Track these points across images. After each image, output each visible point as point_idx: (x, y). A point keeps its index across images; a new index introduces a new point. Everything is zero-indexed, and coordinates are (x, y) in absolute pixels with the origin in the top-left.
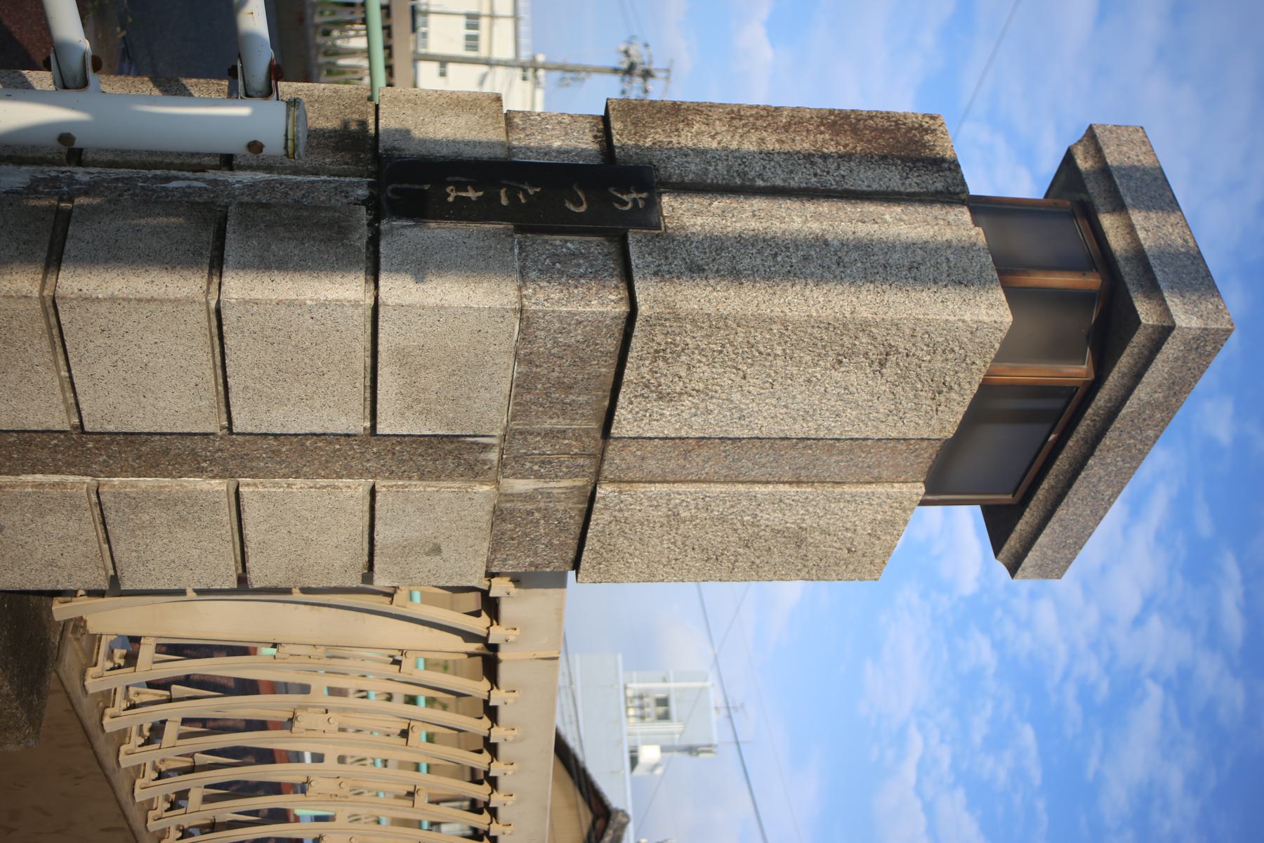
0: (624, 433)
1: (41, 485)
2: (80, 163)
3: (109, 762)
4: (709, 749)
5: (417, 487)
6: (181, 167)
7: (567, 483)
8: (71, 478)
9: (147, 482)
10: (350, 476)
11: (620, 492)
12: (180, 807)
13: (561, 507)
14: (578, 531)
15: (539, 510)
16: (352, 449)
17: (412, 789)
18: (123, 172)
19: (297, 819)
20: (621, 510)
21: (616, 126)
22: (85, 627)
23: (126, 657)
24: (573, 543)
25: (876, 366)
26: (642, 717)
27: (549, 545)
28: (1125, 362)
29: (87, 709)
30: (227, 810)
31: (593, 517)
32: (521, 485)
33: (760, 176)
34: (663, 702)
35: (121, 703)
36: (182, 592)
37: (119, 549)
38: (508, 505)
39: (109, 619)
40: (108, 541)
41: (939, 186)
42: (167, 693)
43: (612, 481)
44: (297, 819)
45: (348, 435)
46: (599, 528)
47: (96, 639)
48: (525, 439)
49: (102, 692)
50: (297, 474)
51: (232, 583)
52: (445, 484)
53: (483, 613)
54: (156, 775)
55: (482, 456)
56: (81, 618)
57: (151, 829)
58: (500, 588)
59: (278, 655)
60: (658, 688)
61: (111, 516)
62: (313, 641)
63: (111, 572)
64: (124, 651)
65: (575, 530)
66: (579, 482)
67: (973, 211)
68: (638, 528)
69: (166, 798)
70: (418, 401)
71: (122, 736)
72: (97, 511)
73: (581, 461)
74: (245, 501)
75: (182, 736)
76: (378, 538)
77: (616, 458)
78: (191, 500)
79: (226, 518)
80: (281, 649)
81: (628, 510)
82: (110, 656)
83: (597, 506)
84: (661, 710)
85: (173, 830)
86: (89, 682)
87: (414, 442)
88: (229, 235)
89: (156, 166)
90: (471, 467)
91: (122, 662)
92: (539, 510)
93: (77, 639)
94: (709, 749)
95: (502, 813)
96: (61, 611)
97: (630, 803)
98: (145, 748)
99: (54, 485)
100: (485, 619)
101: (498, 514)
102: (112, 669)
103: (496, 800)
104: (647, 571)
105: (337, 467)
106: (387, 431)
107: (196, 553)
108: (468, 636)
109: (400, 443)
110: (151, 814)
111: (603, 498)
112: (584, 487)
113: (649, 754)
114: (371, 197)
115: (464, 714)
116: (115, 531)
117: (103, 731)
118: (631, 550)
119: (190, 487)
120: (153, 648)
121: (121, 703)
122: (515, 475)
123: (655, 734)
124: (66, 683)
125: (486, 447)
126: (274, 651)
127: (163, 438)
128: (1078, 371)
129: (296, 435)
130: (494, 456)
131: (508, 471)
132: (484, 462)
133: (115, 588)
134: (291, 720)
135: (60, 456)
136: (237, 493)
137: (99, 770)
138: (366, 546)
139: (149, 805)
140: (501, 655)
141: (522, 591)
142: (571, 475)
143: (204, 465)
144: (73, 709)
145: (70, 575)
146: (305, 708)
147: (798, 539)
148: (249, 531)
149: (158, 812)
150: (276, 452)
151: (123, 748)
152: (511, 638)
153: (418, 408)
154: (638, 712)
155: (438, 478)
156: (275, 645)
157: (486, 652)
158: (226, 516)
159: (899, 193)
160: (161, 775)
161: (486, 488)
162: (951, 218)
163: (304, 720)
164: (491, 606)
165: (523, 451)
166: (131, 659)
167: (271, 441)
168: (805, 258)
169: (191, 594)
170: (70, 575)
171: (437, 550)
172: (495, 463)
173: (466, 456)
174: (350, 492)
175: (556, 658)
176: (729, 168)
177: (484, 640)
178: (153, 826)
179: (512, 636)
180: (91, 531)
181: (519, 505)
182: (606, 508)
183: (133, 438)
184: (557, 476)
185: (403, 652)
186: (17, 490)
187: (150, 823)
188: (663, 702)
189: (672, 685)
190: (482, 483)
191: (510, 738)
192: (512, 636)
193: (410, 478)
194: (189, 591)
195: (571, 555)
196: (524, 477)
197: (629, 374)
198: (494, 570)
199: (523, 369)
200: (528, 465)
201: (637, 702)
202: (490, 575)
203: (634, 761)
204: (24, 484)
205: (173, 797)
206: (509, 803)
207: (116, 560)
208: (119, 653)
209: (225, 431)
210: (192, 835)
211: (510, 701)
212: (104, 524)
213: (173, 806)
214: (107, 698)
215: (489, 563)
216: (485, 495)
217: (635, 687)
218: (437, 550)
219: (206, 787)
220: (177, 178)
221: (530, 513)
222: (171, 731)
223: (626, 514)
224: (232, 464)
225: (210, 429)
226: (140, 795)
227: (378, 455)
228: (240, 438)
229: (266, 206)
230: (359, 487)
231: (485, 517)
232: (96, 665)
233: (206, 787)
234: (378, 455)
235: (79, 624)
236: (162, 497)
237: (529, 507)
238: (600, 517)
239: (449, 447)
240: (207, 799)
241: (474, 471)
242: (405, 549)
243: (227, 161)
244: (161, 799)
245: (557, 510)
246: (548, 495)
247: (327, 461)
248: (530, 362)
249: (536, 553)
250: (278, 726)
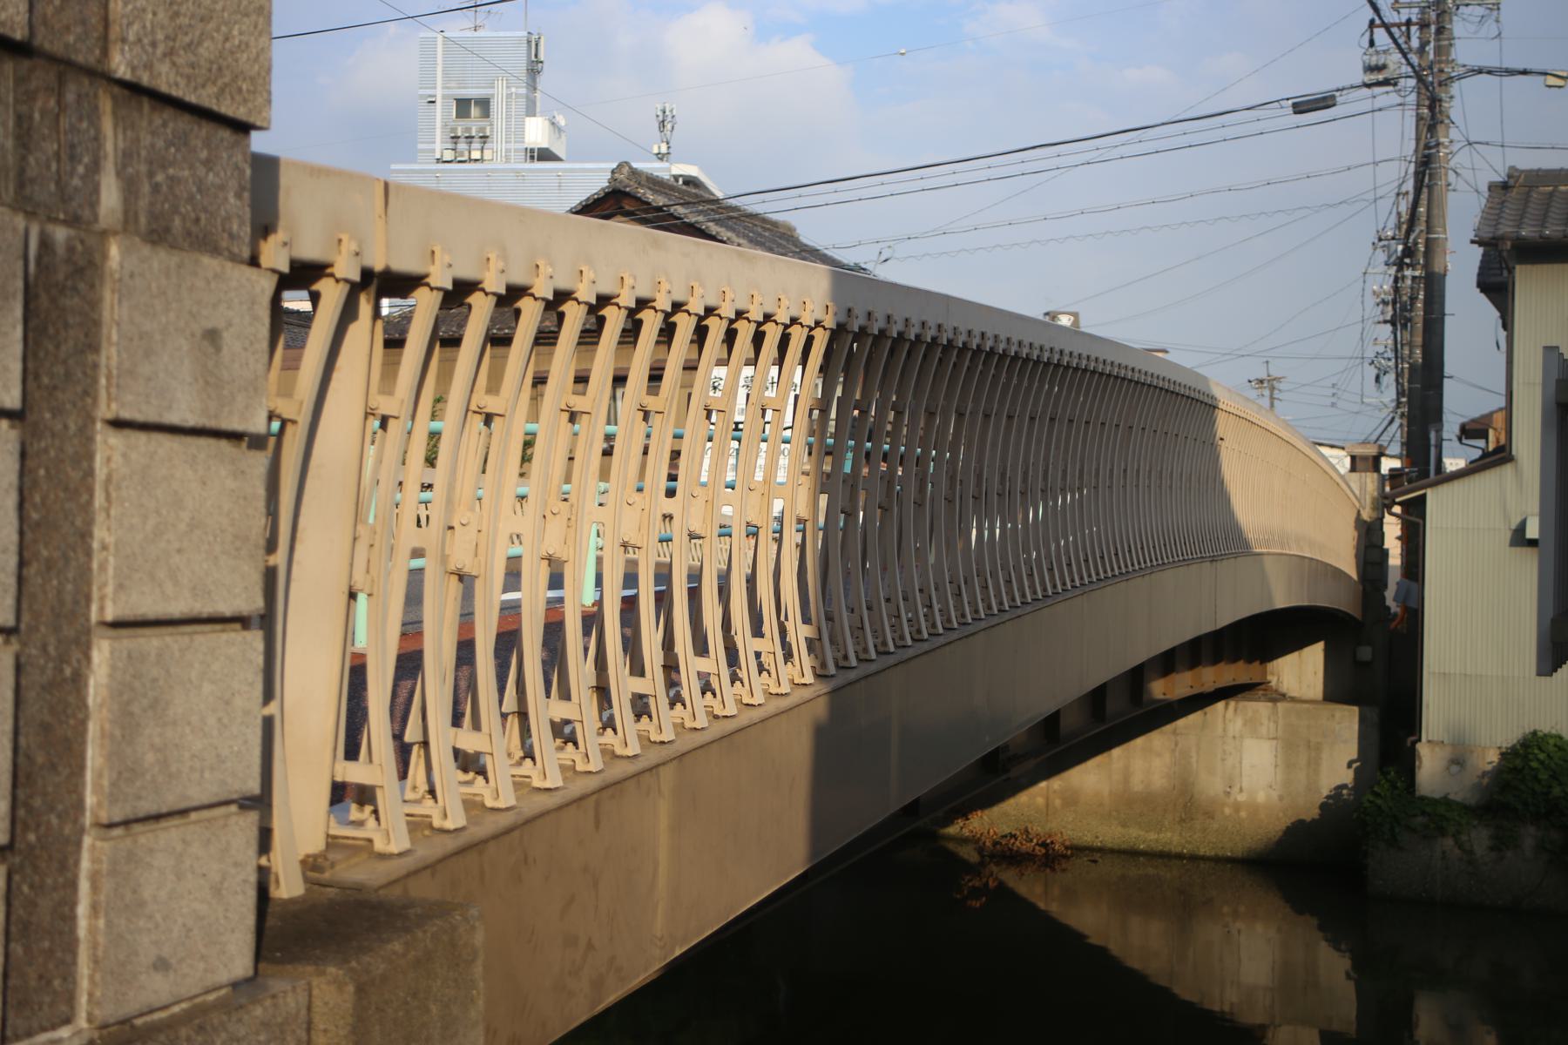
0: (21, 18)
1: (95, 908)
3: (505, 821)
4: (533, 44)
5: (110, 356)
7: (107, 125)
8: (85, 864)
9: (94, 756)
10: (90, 457)
11: (124, 40)
12: (573, 732)
13: (146, 140)
14: (187, 117)
16: (46, 451)
17: (566, 415)
19: (599, 603)
20: (154, 44)
22: (315, 857)
23: (361, 803)
24: (205, 129)
27: (208, 164)
29: (431, 850)
30: (581, 672)
31: (164, 88)
32: (110, 197)
34: (463, 106)
35: (428, 807)
36: (268, 723)
37: (198, 796)
38: (143, 220)
39: (304, 821)
40: (184, 812)
42: (415, 749)
43: (105, 52)
44: (599, 603)
45: (23, 455)
46: (182, 82)
47: (332, 842)
48: (32, 181)
49: (410, 832)
50: (85, 535)
51: (256, 639)
52: (106, 314)
53: (315, 287)
54: (528, 761)
55: (61, 250)
56: (303, 862)
57: (600, 766)
58: (275, 256)
59: (367, 591)
60: (443, 113)
61: (147, 806)
62: (349, 539)
63: (233, 808)
64: (354, 806)
65: (184, 122)
66: (106, 105)
68: (184, 21)
69: (560, 749)
71: (472, 806)
72: (137, 828)
73: (70, 97)
74: (127, 613)
75: (476, 726)
76: (192, 421)
77: (71, 42)
78: (123, 691)
79: (155, 642)
80: (358, 586)
81: (153, 32)
82: (360, 824)
83: (145, 79)
84: (474, 111)
85: (603, 740)
86: (394, 848)
87: (35, 355)
90: (79, 272)
91: (368, 809)
92: (151, 175)
93: (333, 865)
94: (533, 44)
95: (605, 289)
96: (289, 886)
97: (603, 165)
98: (490, 775)
99: (95, 888)
100: (324, 286)
101: (158, 236)
102: (377, 819)
103: (586, 294)
104: (254, 17)
105: (75, 475)
107: (207, 688)
108: (348, 313)
109: (37, 376)
110: (580, 767)
111: (134, 69)
112: (114, 99)
113: (536, 132)
115: (501, 618)
116: (170, 801)
117: (463, 829)
118: (219, 37)
119: (104, 692)
120: (351, 765)
121: (428, 807)
122: (94, 204)
123: (508, 117)
124: (393, 877)
125: (45, 244)
126: (362, 598)
127: (22, 731)
129: (21, 533)
130: (60, 234)
131: (86, 213)
132: (71, 249)
133: (260, 802)
134: (461, 578)
135: (49, 881)
136: (117, 625)
137: (516, 834)
138: (203, 442)
139: (569, 770)
140: (379, 267)
141: (282, 223)
142: (94, 116)
143: (68, 671)
144: (431, 867)
145: (236, 864)
146: (444, 559)
148: (177, 609)
149: (578, 759)
150: (49, 565)
151: (489, 803)
152: (354, 247)
154: (476, 145)
155: (97, 324)
156: (352, 596)
157: (373, 289)
158: (151, 641)
160: (529, 754)
161: (114, 251)
163: (462, 558)
164: (304, 274)
165: (52, 187)
166: (365, 795)
167: (31, 571)
169: (272, 708)
170: (236, 864)
171: (212, 336)
172: (72, 232)
173: (61, 276)
174: (117, 459)
175: (386, 185)
177: (355, 290)
178: (596, 764)
179: (349, 246)
180: (170, 834)
181: (143, 203)
182: (149, 66)
183: (21, 775)
184: (96, 139)
185: (369, 414)
186: (101, 939)
187: (592, 767)
188: (463, 106)
189: (439, 93)
190: (105, 256)
191: (501, 265)
192: (349, 246)
193: (96, 366)
194: (267, 711)
195: (225, 134)
196: (96, 190)
198: (246, 253)
200: (76, 182)
201: (462, 146)
202: (254, 262)
203: (545, 155)
204: (92, 931)
205: (559, 741)
206: (592, 275)
207: (214, 800)
208: (354, 813)
209: (13, 639)
210: (611, 718)
211: (447, 259)
212: (158, 817)
213: (572, 739)
214: (418, 826)
215: (234, 258)
216: (126, 252)
217: (440, 146)
218: (212, 336)
219: (548, 696)
221: (156, 188)
222: (469, 741)
223: (160, 36)
224: (68, 632)
225: (9, 661)
226: (554, 780)
228: (26, 617)
230: (110, 449)
231: (161, 259)
232: (370, 841)
233: (548, 696)
234: (57, 412)
235: (311, 865)
236: (118, 733)
237: (146, 188)
238: (166, 79)
239: (44, 301)
240: (565, 695)
241: (86, 268)
242: (210, 381)
244: (561, 755)
245: (153, 146)
246: (127, 156)
247: (66, 489)
249: (222, 187)
250: (468, 596)
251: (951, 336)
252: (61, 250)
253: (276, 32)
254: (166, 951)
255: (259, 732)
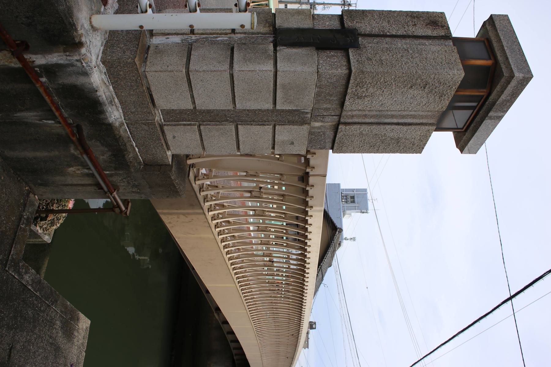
2: (194, 34)
6: (221, 34)
15: (322, 132)
18: (204, 36)
21: (345, 17)
25: (422, 88)
26: (346, 202)
28: (498, 88)
32: (317, 124)
33: (388, 32)
34: (353, 197)
41: (443, 34)
55: (306, 116)
67: (453, 41)
70: (288, 99)
73: (334, 117)
88: (235, 52)
89: (214, 34)
101: (310, 133)
106: (279, 108)
114: (273, 40)
122: (315, 121)
125: (307, 113)
128: (482, 92)
132: (307, 118)
147: (398, 140)
148: (240, 138)
153: (288, 101)
159: (431, 36)
162: (446, 44)
168: (402, 56)
171: (292, 143)
176: (379, 29)
188: (353, 197)
196: (318, 122)
197: (349, 91)
199: (318, 90)
218: (292, 143)
220: (219, 37)
221: (319, 133)
227: (276, 116)
229: (245, 44)
231: (306, 134)
241: (303, 122)
243: (233, 31)
248: (320, 88)
251: (308, 256)
252: (306, 116)
253: (190, 107)
254: (176, 138)
255: (241, 147)
